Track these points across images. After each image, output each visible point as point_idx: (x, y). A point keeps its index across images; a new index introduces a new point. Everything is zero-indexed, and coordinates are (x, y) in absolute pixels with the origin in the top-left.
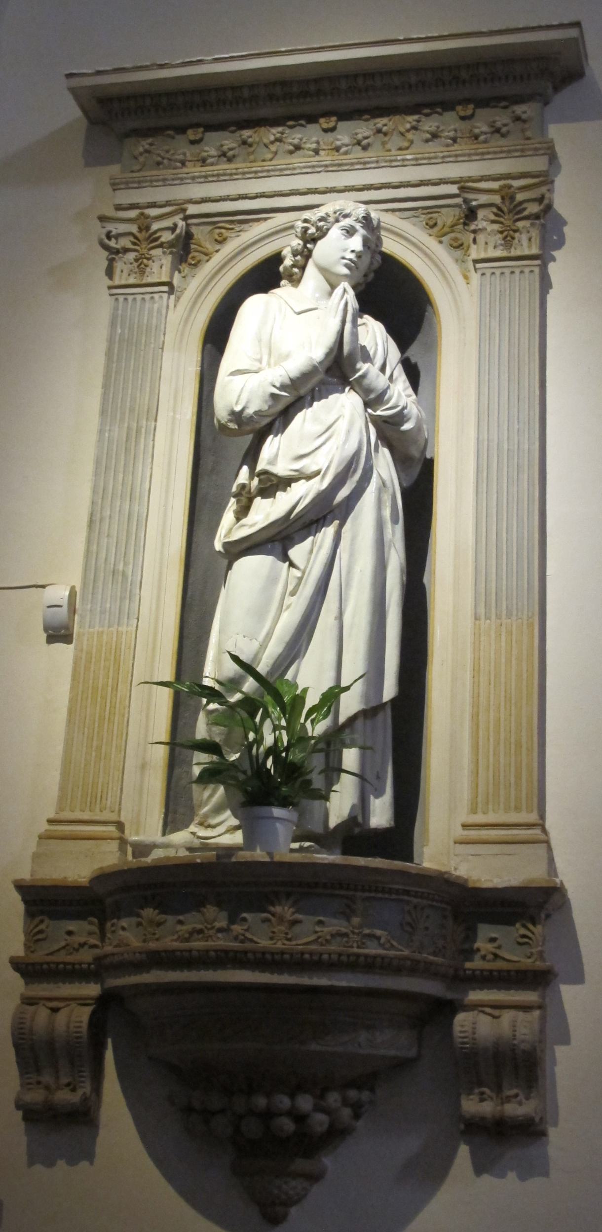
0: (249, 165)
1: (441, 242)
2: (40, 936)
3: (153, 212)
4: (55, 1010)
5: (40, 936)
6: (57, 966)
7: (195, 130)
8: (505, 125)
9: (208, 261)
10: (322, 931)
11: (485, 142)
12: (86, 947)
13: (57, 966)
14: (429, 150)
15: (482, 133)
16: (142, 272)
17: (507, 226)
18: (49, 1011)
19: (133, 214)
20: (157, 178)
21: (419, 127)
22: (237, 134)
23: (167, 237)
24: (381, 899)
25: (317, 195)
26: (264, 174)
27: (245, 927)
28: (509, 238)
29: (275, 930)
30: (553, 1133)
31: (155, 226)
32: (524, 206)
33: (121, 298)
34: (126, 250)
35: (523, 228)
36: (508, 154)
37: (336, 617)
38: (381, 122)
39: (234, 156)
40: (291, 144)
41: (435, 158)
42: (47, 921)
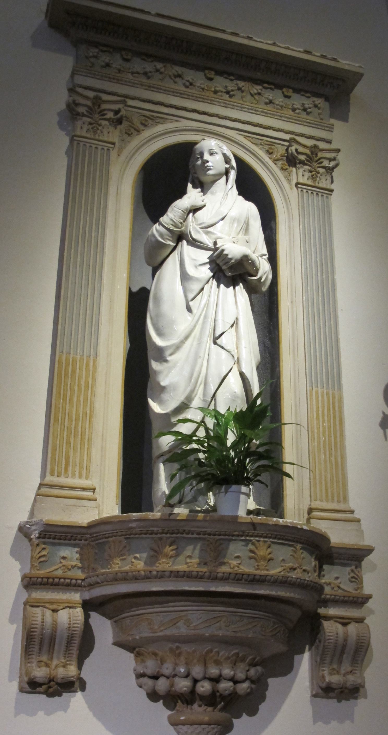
0: (242, 102)
1: (275, 164)
2: (42, 559)
3: (105, 97)
4: (55, 611)
5: (42, 559)
6: (37, 579)
7: (288, 89)
8: (310, 108)
9: (138, 135)
10: (191, 562)
11: (298, 114)
12: (76, 568)
13: (37, 579)
14: (266, 108)
15: (298, 108)
16: (95, 133)
17: (95, 121)
18: (51, 612)
19: (91, 94)
20: (169, 89)
21: (262, 94)
22: (235, 82)
23: (110, 115)
24: (132, 538)
25: (251, 126)
26: (186, 96)
27: (239, 562)
28: (95, 128)
29: (259, 564)
30: (366, 686)
31: (104, 106)
32: (105, 112)
33: (82, 144)
34: (84, 115)
35: (104, 125)
36: (309, 124)
37: (161, 364)
38: (241, 84)
39: (234, 95)
40: (267, 98)
41: (252, 109)
42: (48, 548)
